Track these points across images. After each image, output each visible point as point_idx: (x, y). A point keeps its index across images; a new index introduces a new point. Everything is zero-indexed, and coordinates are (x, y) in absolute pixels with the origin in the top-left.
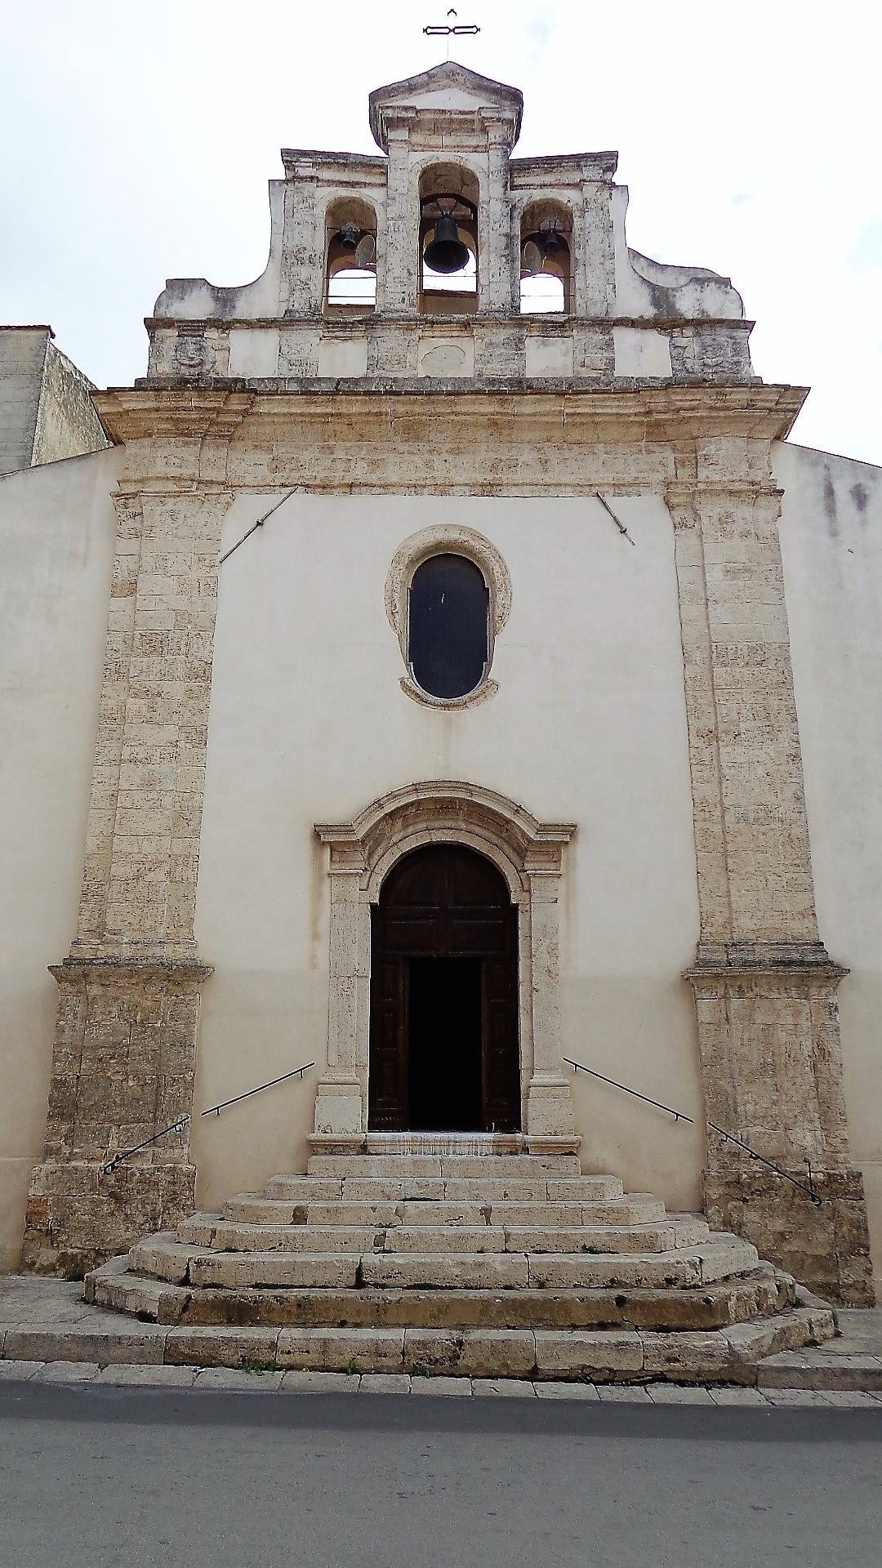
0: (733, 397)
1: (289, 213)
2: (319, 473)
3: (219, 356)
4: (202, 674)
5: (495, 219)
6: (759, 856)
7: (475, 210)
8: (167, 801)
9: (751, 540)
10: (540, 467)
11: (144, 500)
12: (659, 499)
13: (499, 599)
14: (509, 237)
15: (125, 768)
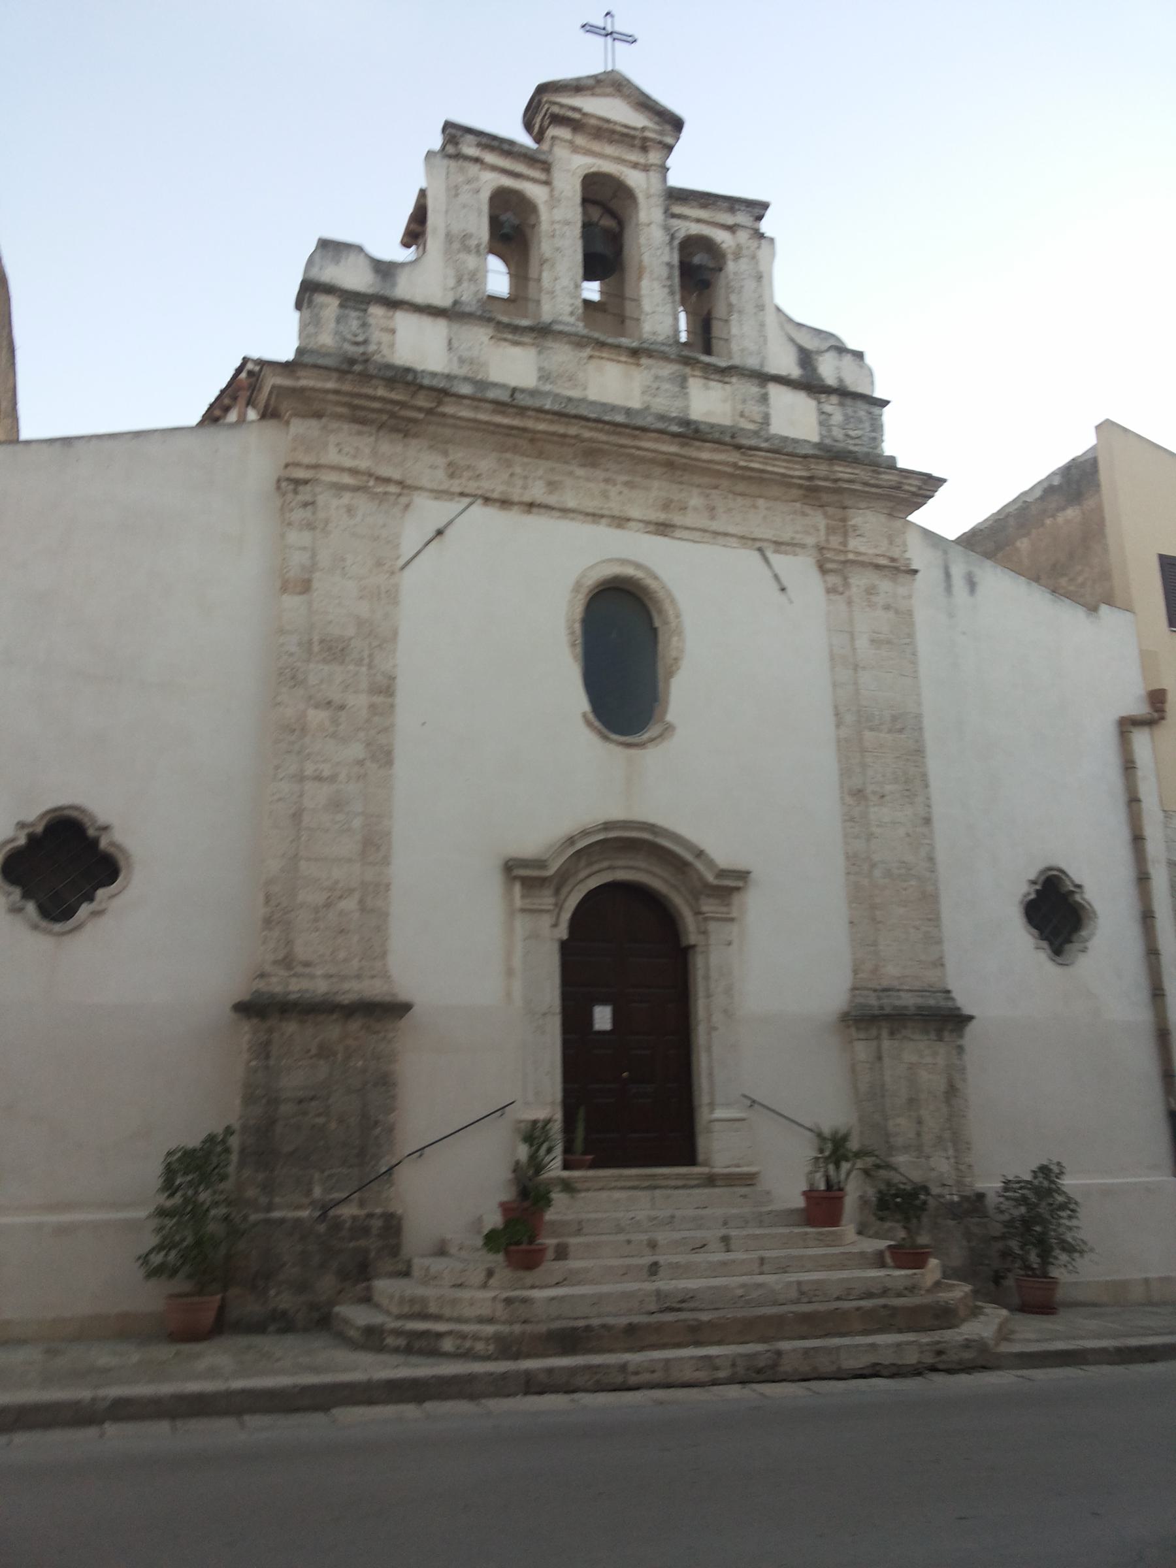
2: (497, 487)
4: (386, 689)
7: (621, 224)
11: (318, 489)
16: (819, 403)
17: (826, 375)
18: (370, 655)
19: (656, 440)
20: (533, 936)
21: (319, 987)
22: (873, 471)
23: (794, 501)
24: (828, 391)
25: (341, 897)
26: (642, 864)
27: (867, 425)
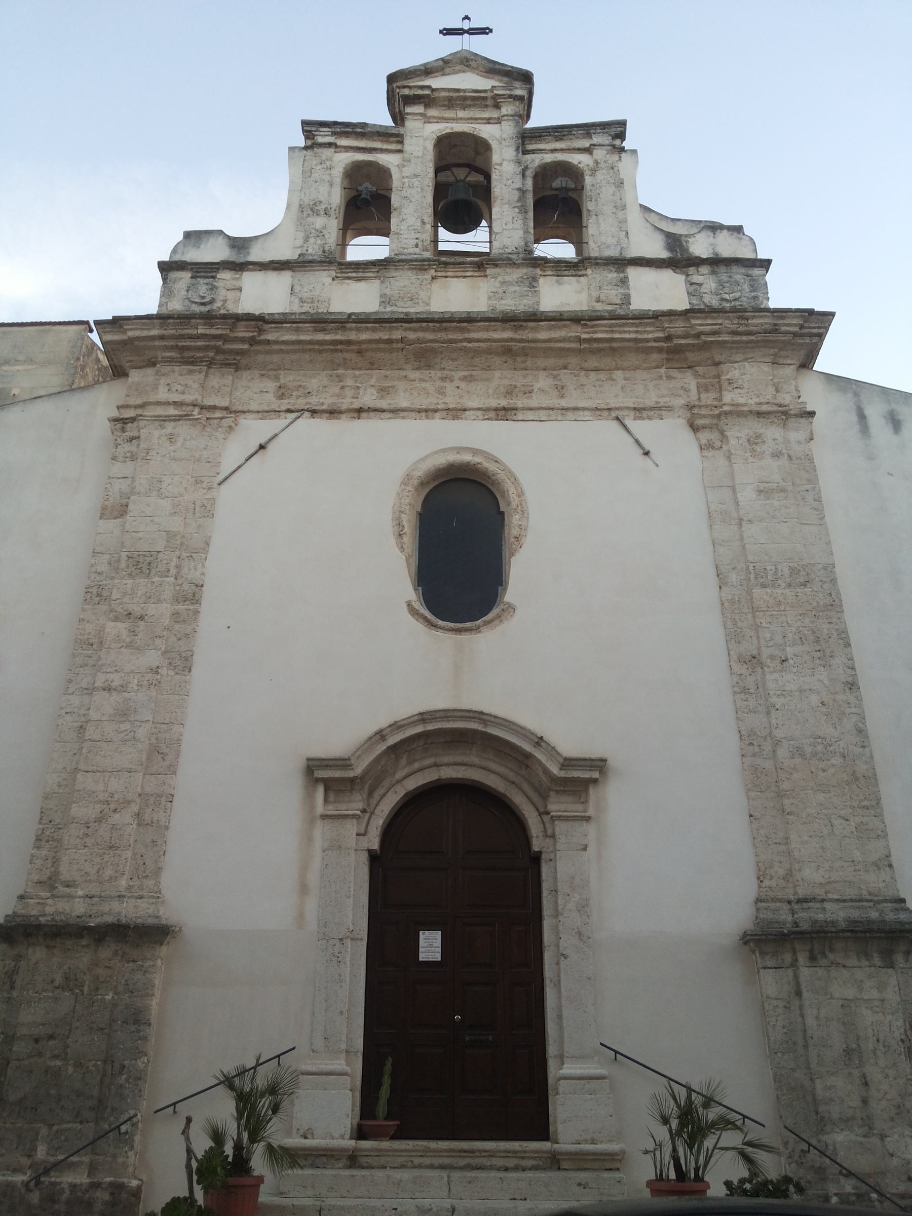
0: (755, 321)
1: (307, 173)
2: (327, 401)
3: (231, 295)
4: (191, 597)
5: (508, 177)
6: (821, 797)
7: (488, 177)
8: (142, 732)
9: (784, 461)
10: (556, 393)
11: (142, 424)
12: (682, 422)
13: (513, 521)
14: (522, 191)
15: (98, 697)
16: (688, 275)
17: (720, 262)
18: (178, 567)
19: (487, 329)
20: (335, 846)
21: (76, 908)
22: (739, 318)
23: (657, 367)
24: (698, 262)
25: (115, 811)
26: (475, 760)
27: (746, 287)
